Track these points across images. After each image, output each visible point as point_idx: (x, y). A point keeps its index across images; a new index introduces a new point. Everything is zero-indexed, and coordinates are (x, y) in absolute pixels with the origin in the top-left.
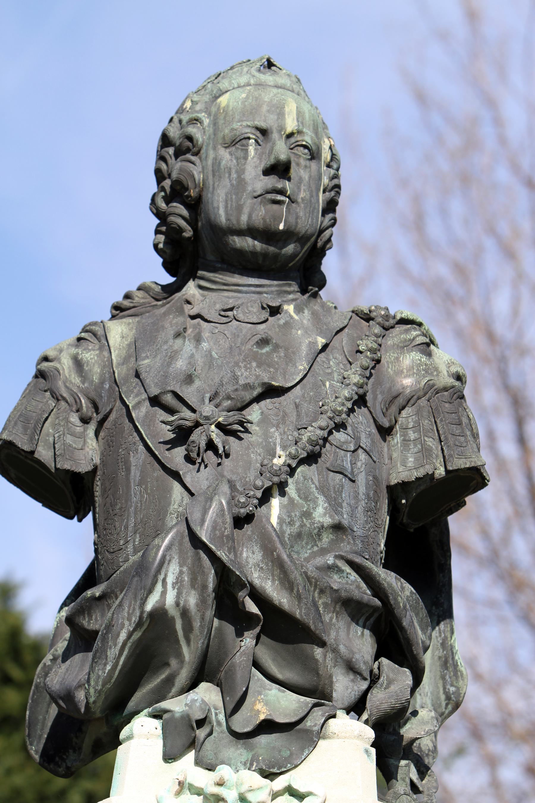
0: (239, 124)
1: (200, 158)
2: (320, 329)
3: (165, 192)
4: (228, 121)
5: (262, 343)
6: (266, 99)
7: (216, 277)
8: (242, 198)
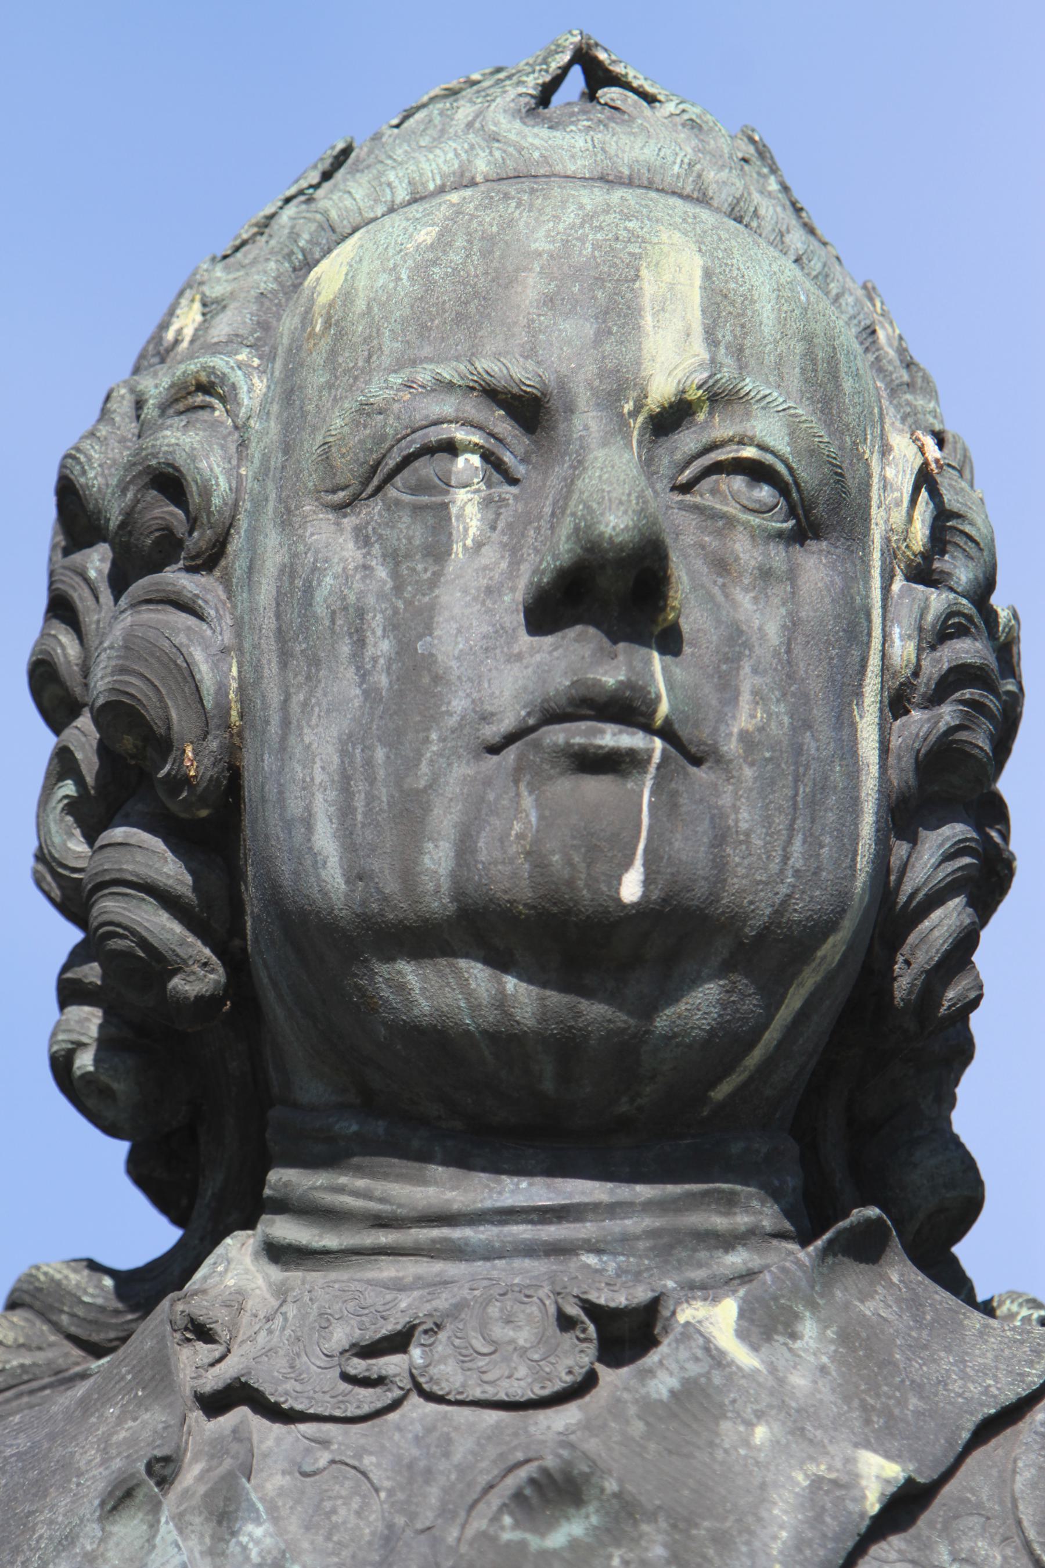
0: (396, 379)
1: (226, 581)
2: (887, 1413)
3: (80, 782)
4: (347, 371)
5: (546, 1500)
6: (540, 243)
7: (341, 1190)
8: (419, 755)
